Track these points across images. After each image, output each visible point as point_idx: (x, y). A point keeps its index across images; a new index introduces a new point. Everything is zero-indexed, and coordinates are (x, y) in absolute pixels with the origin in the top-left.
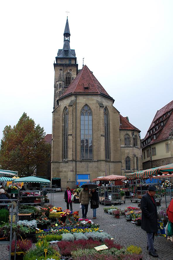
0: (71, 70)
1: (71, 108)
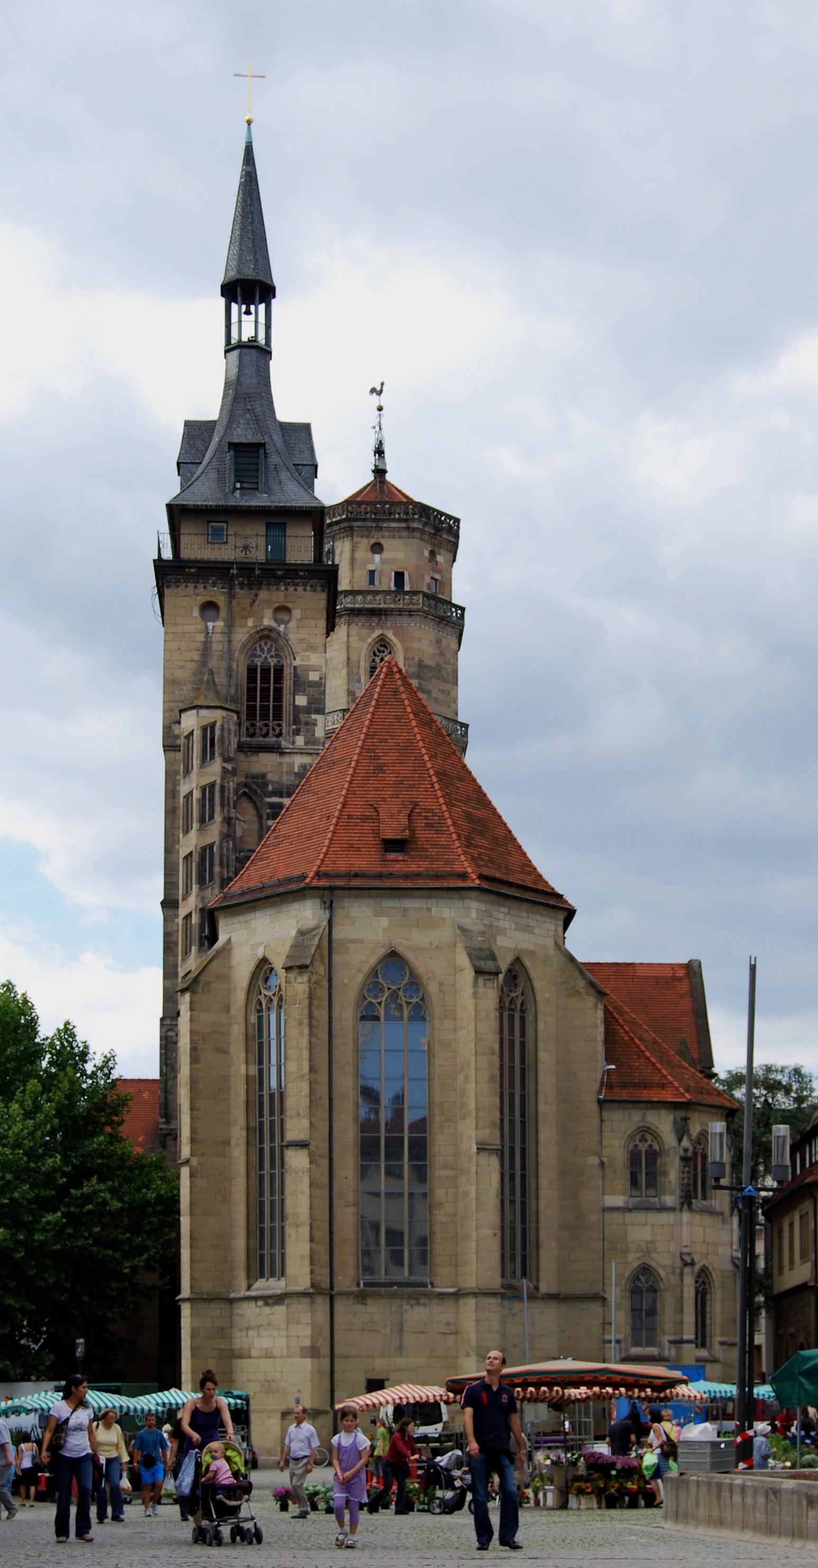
0: (288, 610)
1: (299, 986)
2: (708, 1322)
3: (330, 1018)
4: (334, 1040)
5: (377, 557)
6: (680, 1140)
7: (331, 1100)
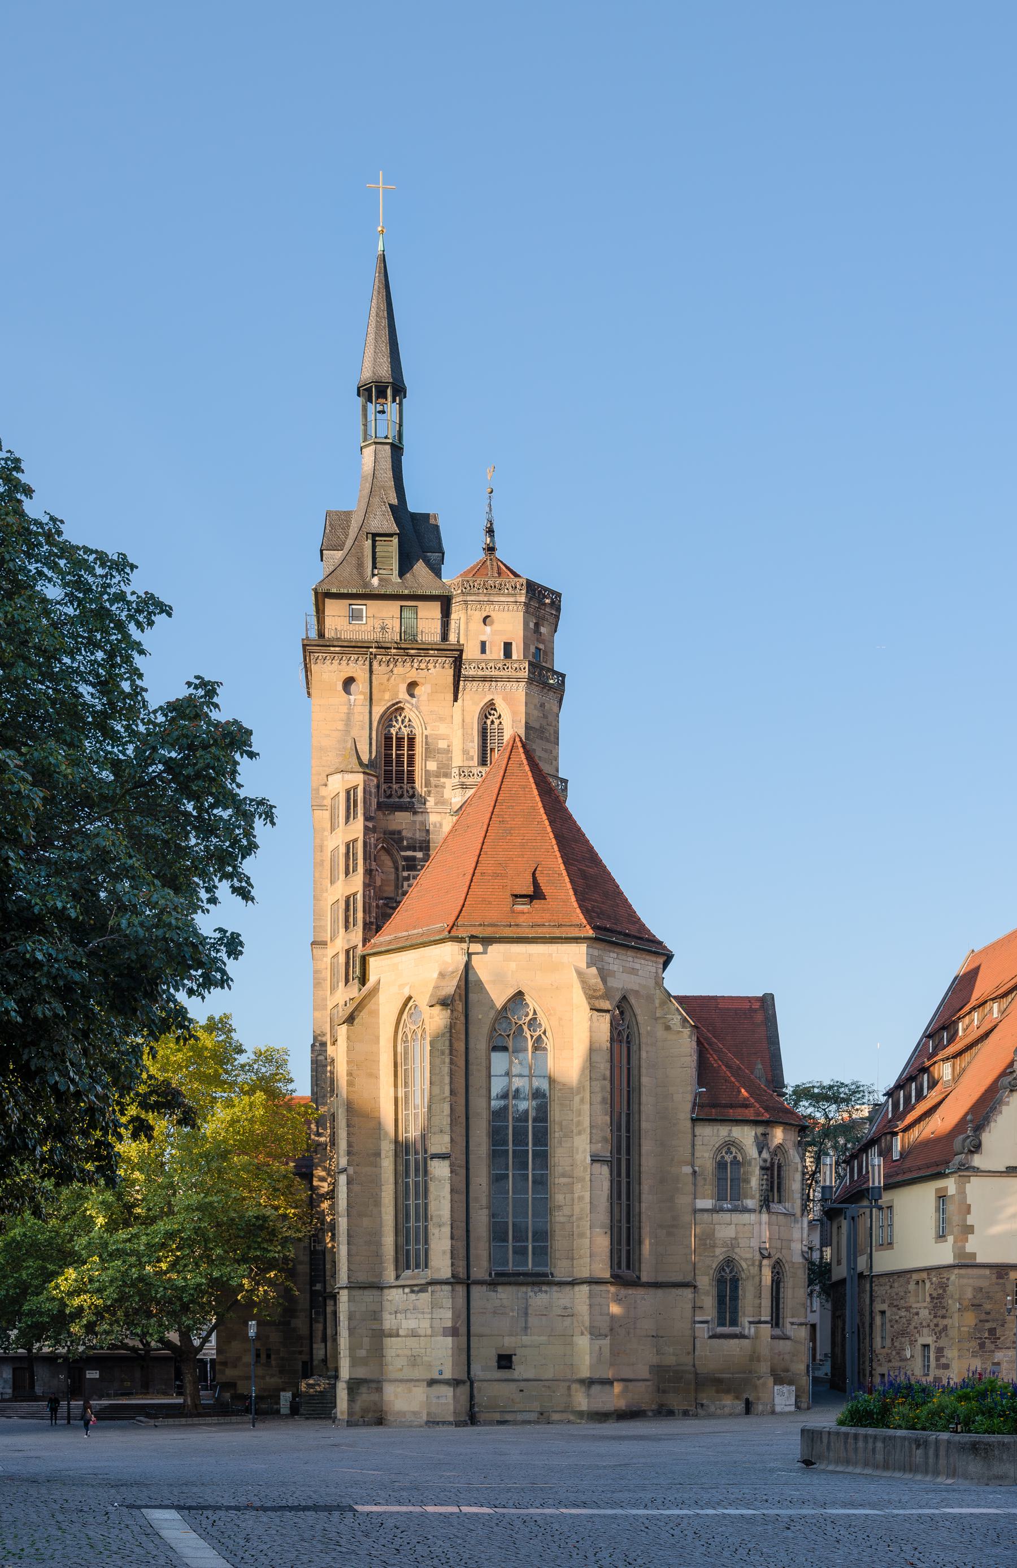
2: (781, 1306)
3: (467, 1048)
4: (470, 1067)
5: (488, 629)
6: (760, 1153)
7: (467, 1118)
